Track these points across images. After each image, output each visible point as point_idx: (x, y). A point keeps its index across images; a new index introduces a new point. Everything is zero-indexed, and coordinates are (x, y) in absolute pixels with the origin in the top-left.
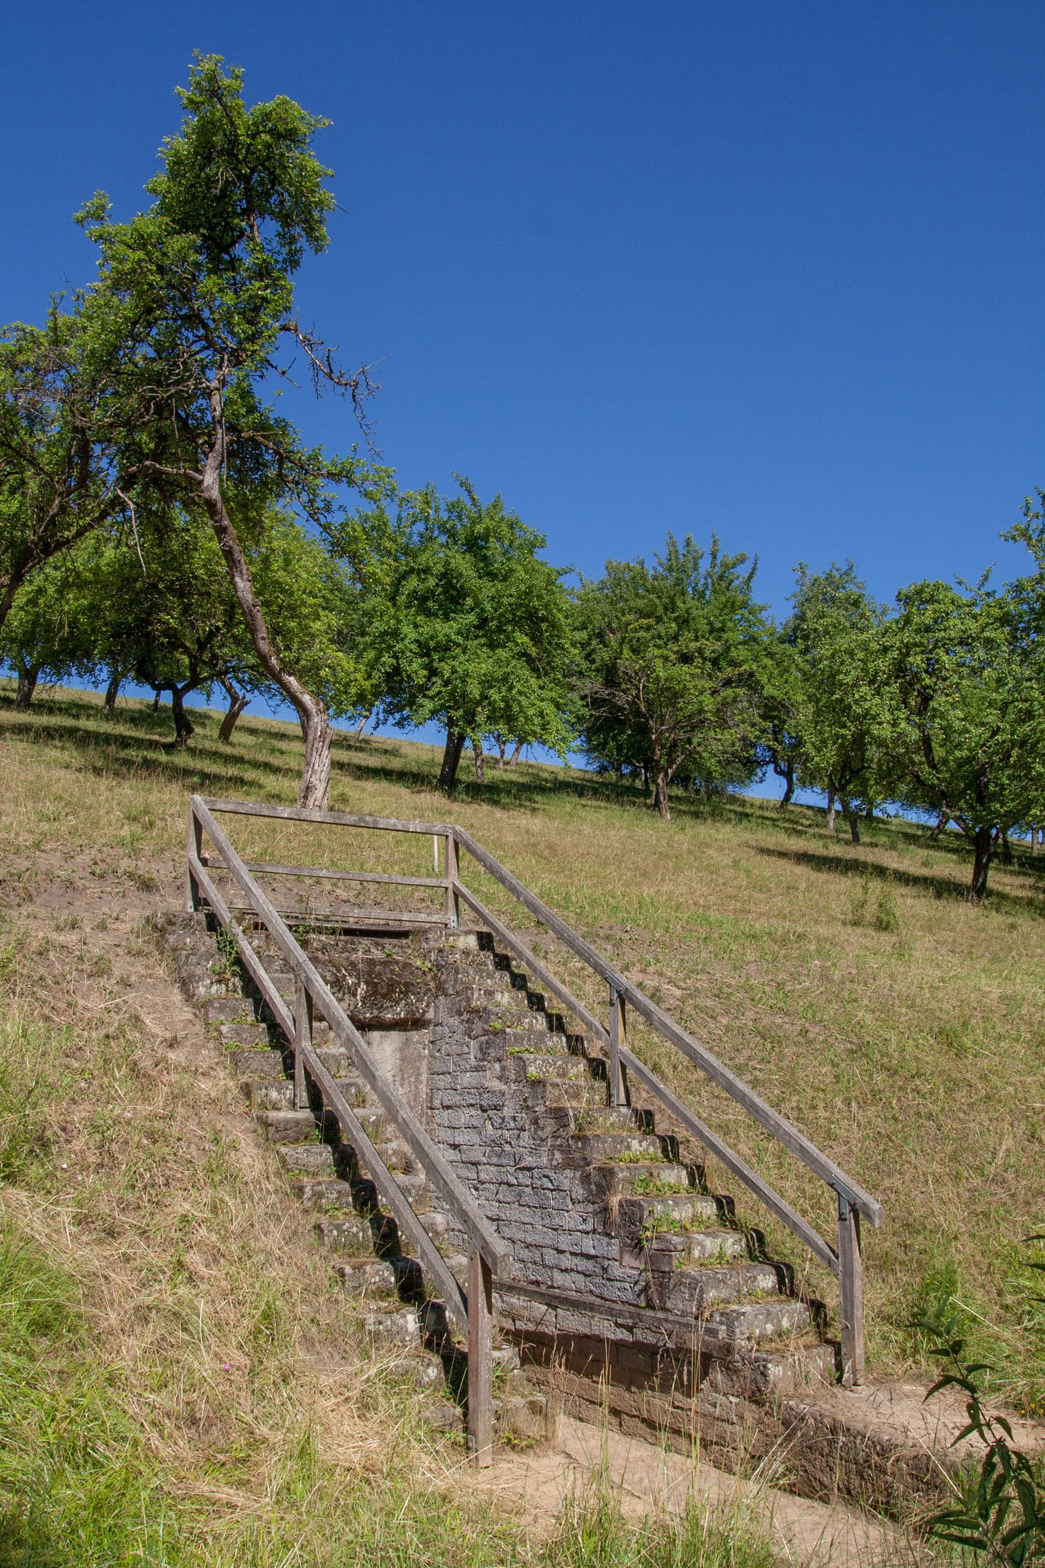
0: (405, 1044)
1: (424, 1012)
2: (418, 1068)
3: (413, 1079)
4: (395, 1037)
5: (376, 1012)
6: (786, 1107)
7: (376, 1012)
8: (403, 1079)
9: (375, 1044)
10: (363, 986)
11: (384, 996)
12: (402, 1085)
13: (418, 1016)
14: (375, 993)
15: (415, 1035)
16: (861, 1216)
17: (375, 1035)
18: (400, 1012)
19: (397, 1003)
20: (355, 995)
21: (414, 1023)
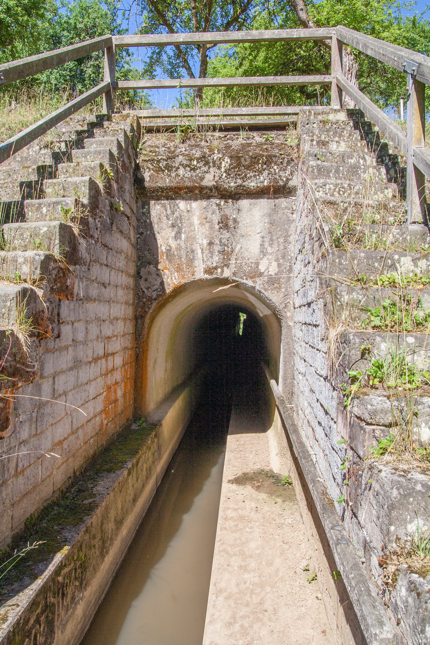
0: (274, 210)
1: (288, 180)
2: (287, 231)
3: (281, 240)
4: (264, 205)
5: (239, 182)
6: (44, 113)
7: (239, 182)
8: (271, 240)
9: (244, 210)
10: (227, 159)
11: (248, 168)
12: (271, 245)
13: (281, 183)
14: (239, 165)
15: (283, 202)
16: (344, 93)
17: (244, 203)
18: (263, 180)
19: (261, 172)
20: (219, 168)
21: (281, 191)
